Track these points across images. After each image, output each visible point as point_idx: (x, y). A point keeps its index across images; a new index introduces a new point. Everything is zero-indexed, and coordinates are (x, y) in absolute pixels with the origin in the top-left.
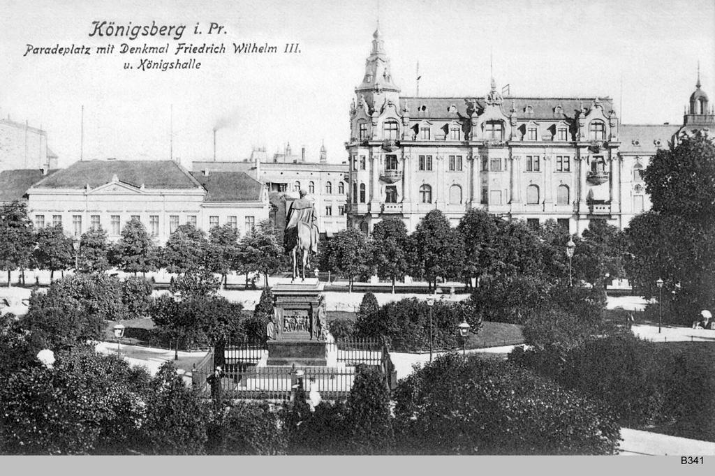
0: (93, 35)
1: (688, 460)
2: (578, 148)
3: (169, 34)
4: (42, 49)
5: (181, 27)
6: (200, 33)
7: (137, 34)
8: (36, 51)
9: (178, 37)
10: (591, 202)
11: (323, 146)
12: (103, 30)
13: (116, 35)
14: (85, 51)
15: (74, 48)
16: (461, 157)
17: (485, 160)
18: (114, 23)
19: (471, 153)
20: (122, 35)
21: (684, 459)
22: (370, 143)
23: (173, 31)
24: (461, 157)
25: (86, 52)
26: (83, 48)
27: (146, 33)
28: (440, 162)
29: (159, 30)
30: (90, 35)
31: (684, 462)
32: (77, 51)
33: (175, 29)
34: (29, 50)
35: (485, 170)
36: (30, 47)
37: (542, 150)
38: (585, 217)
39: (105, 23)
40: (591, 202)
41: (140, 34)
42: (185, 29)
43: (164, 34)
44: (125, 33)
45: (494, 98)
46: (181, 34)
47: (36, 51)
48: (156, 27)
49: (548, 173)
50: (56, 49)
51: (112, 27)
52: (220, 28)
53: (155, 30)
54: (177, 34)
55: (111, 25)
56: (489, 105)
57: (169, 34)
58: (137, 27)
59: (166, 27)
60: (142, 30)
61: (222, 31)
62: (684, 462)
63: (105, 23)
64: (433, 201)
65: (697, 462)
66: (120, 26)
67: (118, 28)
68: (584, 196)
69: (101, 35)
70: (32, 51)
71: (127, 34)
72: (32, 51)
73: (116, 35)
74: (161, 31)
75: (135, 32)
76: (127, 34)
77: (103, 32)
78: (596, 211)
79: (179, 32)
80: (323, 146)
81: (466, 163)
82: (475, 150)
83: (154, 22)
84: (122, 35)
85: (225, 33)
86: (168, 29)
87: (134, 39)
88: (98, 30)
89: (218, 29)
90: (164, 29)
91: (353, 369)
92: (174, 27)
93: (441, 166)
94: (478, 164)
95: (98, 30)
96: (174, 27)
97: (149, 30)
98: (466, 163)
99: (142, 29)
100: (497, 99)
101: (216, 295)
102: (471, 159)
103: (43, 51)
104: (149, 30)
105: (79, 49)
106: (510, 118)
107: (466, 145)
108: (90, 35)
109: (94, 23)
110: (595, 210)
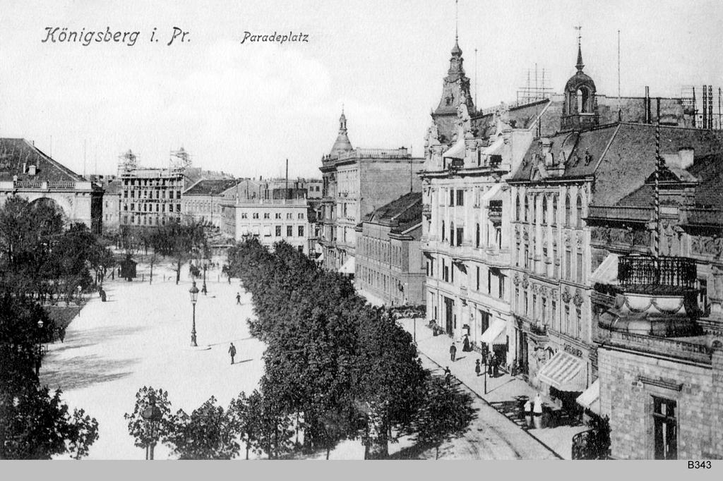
0: (46, 41)
1: (695, 465)
3: (123, 40)
5: (91, 33)
7: (90, 40)
8: (253, 39)
9: (131, 43)
11: (343, 115)
14: (302, 38)
15: (292, 35)
18: (66, 29)
20: (75, 40)
21: (691, 463)
23: (128, 36)
26: (301, 35)
27: (99, 39)
29: (113, 36)
30: (43, 41)
32: (295, 38)
41: (93, 41)
44: (77, 39)
47: (171, 43)
48: (109, 33)
50: (274, 37)
52: (184, 34)
55: (65, 31)
57: (123, 40)
58: (91, 33)
60: (95, 36)
61: (186, 37)
65: (704, 466)
66: (72, 32)
67: (71, 34)
72: (249, 38)
73: (69, 40)
75: (88, 38)
77: (56, 37)
79: (133, 38)
80: (343, 115)
83: (108, 28)
88: (50, 36)
89: (182, 34)
90: (118, 34)
91: (704, 330)
95: (50, 36)
97: (103, 36)
103: (261, 39)
104: (103, 36)
105: (296, 36)
108: (43, 41)
109: (47, 29)
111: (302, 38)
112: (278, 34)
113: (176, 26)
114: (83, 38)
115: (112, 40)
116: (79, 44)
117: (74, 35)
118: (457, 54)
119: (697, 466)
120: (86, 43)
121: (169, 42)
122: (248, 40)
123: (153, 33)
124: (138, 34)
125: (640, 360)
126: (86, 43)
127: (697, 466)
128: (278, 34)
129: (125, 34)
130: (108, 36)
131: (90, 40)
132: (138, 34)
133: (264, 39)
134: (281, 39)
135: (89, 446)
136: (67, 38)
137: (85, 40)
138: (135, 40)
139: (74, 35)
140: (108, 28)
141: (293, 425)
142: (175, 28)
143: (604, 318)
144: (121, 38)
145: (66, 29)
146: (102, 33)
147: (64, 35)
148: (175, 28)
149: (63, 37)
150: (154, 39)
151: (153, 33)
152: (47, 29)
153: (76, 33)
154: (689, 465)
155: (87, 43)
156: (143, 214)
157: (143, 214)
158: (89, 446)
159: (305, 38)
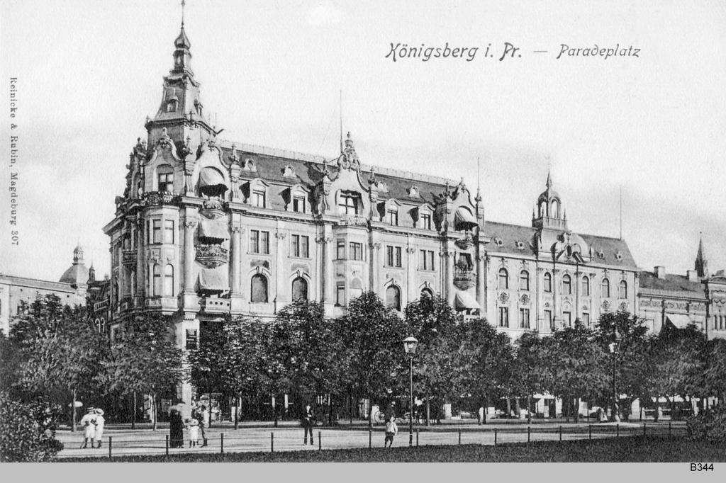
2: (321, 223)
3: (461, 56)
4: (579, 50)
6: (492, 56)
7: (430, 55)
9: (470, 58)
10: (203, 293)
13: (409, 56)
16: (268, 233)
17: (339, 245)
18: (407, 45)
19: (323, 233)
20: (414, 56)
22: (184, 201)
23: (466, 52)
24: (268, 233)
25: (634, 55)
27: (438, 55)
28: (280, 241)
29: (452, 52)
31: (693, 469)
33: (468, 51)
34: (506, 52)
35: (339, 260)
37: (272, 223)
38: (193, 316)
40: (203, 293)
42: (478, 51)
43: (456, 56)
44: (417, 55)
45: (351, 160)
49: (412, 270)
51: (405, 49)
52: (515, 50)
53: (447, 52)
54: (470, 56)
55: (404, 47)
56: (345, 168)
57: (461, 56)
58: (587, 49)
59: (605, 50)
60: (434, 52)
62: (693, 469)
63: (398, 45)
64: (271, 299)
67: (411, 49)
68: (191, 284)
70: (567, 52)
71: (419, 55)
72: (567, 52)
73: (409, 56)
74: (453, 53)
76: (419, 55)
77: (397, 57)
78: (209, 308)
79: (472, 54)
81: (314, 248)
82: (328, 228)
83: (447, 44)
84: (414, 56)
85: (520, 56)
86: (607, 51)
92: (467, 49)
93: (413, 261)
94: (331, 248)
96: (467, 49)
98: (314, 248)
99: (434, 50)
100: (354, 162)
101: (56, 457)
102: (322, 241)
103: (581, 52)
106: (369, 191)
107: (320, 223)
110: (208, 306)
113: (508, 42)
115: (598, 54)
116: (418, 60)
118: (181, 48)
119: (700, 469)
120: (426, 58)
121: (558, 56)
122: (565, 55)
123: (488, 48)
124: (477, 49)
126: (426, 58)
127: (700, 469)
131: (430, 55)
132: (477, 49)
133: (586, 53)
134: (605, 54)
138: (474, 55)
139: (414, 51)
140: (447, 44)
141: (346, 194)
145: (407, 45)
147: (404, 51)
150: (489, 55)
151: (488, 48)
153: (584, 55)
154: (691, 467)
155: (471, 58)
156: (411, 427)
157: (411, 427)
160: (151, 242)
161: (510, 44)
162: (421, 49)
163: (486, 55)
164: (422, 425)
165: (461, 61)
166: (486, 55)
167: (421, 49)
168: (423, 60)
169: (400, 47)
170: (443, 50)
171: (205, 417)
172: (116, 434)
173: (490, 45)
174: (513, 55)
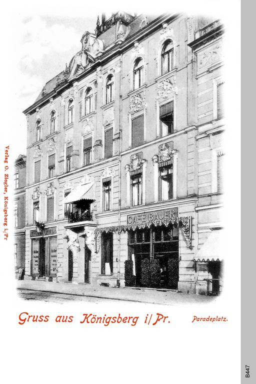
3: (128, 322)
4: (130, 318)
12: (89, 320)
14: (223, 319)
18: (105, 315)
23: (131, 320)
27: (70, 320)
30: (81, 322)
34: (194, 319)
36: (161, 317)
39: (91, 315)
44: (102, 321)
46: (136, 322)
48: (121, 318)
52: (165, 318)
53: (120, 319)
57: (128, 322)
58: (109, 318)
60: (112, 320)
63: (91, 315)
66: (59, 322)
67: (98, 318)
69: (88, 322)
71: (103, 322)
73: (97, 322)
74: (123, 320)
75: (108, 321)
77: (89, 320)
79: (135, 321)
83: (119, 314)
84: (100, 322)
85: (169, 322)
86: (128, 319)
87: (41, 321)
88: (86, 319)
89: (164, 318)
92: (132, 317)
95: (86, 319)
96: (132, 317)
97: (116, 320)
104: (116, 320)
108: (81, 322)
109: (84, 315)
111: (223, 319)
112: (210, 318)
114: (105, 321)
117: (64, 320)
120: (107, 324)
123: (147, 317)
124: (137, 318)
125: (51, 84)
128: (210, 318)
129: (130, 318)
130: (120, 319)
132: (137, 318)
135: (167, 225)
136: (105, 319)
137: (133, 322)
139: (99, 319)
140: (119, 314)
142: (158, 314)
143: (6, 185)
144: (127, 321)
146: (116, 318)
148: (158, 314)
149: (93, 320)
152: (84, 315)
153: (33, 321)
158: (167, 225)
159: (225, 320)
160: (88, 112)
161: (161, 315)
162: (104, 318)
163: (145, 322)
164: (36, 109)
165: (128, 325)
166: (145, 322)
167: (104, 318)
168: (132, 325)
169: (92, 316)
170: (117, 318)
171: (129, 177)
172: (181, 206)
173: (148, 315)
174: (164, 322)
